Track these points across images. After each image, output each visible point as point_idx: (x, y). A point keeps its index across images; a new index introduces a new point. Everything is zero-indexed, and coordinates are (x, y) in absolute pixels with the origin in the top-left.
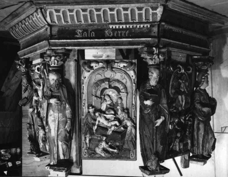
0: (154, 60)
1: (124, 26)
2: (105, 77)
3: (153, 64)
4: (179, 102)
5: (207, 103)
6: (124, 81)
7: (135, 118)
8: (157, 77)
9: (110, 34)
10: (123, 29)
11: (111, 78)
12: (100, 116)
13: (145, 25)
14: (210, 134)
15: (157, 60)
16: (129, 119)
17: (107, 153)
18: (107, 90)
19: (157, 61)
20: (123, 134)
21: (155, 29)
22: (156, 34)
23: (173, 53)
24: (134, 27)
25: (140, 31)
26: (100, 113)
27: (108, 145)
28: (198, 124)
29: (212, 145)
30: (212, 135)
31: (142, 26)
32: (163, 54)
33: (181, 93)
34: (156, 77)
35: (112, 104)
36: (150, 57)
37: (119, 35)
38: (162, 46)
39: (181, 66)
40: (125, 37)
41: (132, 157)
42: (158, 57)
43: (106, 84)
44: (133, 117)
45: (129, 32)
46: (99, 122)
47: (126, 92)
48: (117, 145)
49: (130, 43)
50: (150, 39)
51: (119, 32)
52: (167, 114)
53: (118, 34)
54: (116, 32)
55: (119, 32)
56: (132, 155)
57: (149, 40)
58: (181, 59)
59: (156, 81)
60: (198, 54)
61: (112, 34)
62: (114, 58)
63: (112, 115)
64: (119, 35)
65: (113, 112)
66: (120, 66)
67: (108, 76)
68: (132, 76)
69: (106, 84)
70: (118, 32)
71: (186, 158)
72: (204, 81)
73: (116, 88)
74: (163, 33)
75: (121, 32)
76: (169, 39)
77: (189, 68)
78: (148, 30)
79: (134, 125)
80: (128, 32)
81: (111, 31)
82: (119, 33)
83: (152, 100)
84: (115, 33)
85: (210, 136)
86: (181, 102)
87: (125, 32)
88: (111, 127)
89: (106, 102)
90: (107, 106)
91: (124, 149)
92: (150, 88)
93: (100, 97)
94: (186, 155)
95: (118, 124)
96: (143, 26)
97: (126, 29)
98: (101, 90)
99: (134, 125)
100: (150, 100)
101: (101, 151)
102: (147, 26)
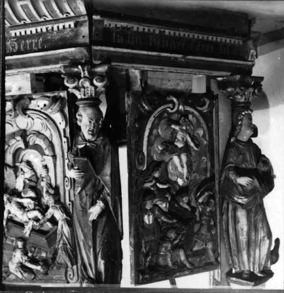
0: (82, 90)
1: (34, 30)
2: (18, 127)
3: (83, 97)
4: (176, 168)
5: (253, 167)
6: (47, 134)
7: (71, 203)
8: (90, 122)
9: (14, 48)
10: (32, 36)
11: (27, 129)
12: (10, 202)
13: (67, 25)
14: (260, 230)
15: (89, 89)
16: (58, 206)
17: (25, 272)
18: (23, 153)
19: (90, 90)
20: (51, 237)
21: (85, 30)
22: (87, 40)
23: (150, 75)
24: (49, 29)
25: (60, 37)
26: (8, 196)
27: (26, 257)
28: (235, 210)
29: (266, 253)
30: (263, 231)
31: (61, 26)
32: (101, 77)
33: (178, 152)
34: (88, 123)
35: (34, 179)
36: (75, 84)
37: (28, 47)
38: (99, 62)
39: (176, 97)
40: (36, 49)
41: (71, 279)
42: (92, 84)
43: (18, 141)
44: (68, 202)
45: (43, 39)
46: (9, 213)
47: (52, 154)
48: (42, 257)
49: (45, 61)
50: (73, 49)
51: (27, 41)
52: (109, 195)
53: (25, 45)
54: (23, 42)
55: (27, 41)
56: (71, 276)
57: (72, 52)
58: (178, 84)
59: (89, 130)
60: (224, 73)
61: (16, 48)
62: (29, 92)
63: (29, 200)
64: (28, 47)
65: (32, 194)
66: (39, 106)
67: (23, 126)
68: (60, 123)
69: (18, 141)
70: (27, 43)
71: (216, 277)
72: (241, 125)
73: (36, 147)
74: (100, 36)
75: (30, 41)
76: (115, 47)
77: (204, 101)
78: (73, 33)
79: (69, 218)
80: (41, 39)
81: (15, 41)
82: (28, 44)
83: (77, 169)
84: (21, 44)
85: (262, 234)
86: (180, 169)
87: (36, 40)
88: (27, 222)
89: (24, 174)
90: (25, 183)
91: (58, 265)
92: (83, 144)
93: (11, 165)
94: (216, 271)
95: (40, 216)
96: (64, 26)
97: (38, 35)
98: (11, 152)
99: (69, 218)
100: (74, 169)
101: (16, 268)
102: (70, 25)
